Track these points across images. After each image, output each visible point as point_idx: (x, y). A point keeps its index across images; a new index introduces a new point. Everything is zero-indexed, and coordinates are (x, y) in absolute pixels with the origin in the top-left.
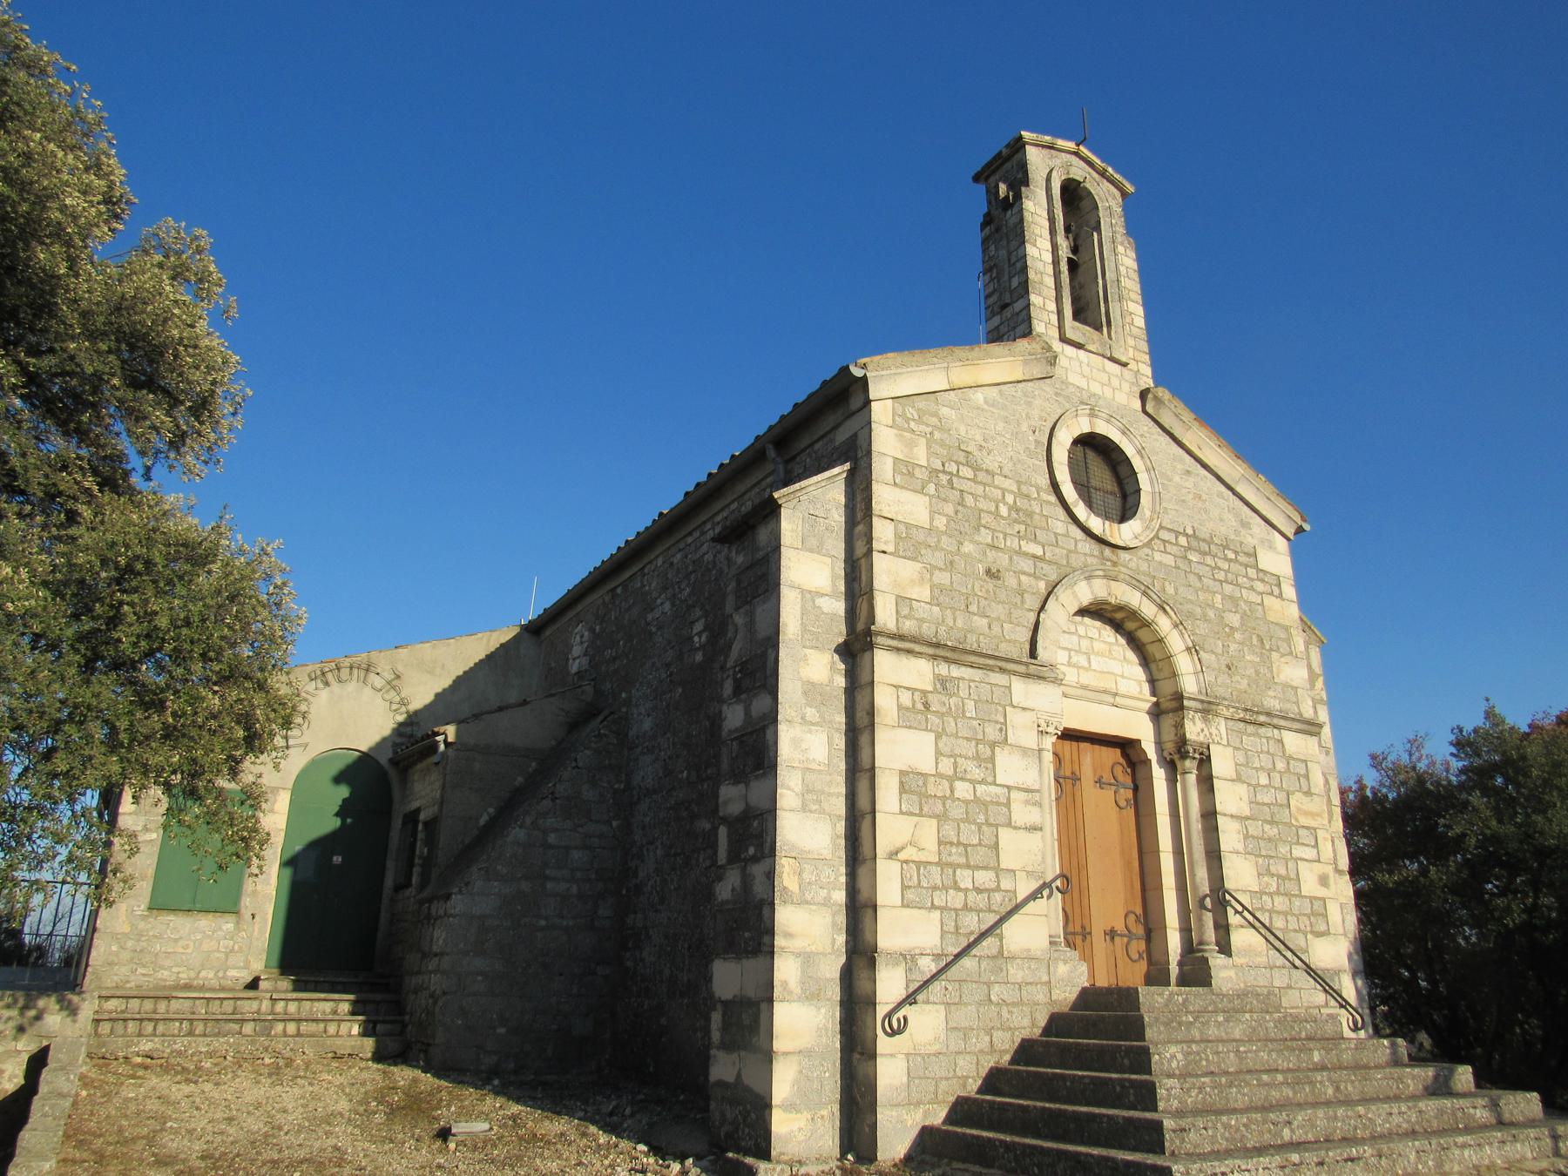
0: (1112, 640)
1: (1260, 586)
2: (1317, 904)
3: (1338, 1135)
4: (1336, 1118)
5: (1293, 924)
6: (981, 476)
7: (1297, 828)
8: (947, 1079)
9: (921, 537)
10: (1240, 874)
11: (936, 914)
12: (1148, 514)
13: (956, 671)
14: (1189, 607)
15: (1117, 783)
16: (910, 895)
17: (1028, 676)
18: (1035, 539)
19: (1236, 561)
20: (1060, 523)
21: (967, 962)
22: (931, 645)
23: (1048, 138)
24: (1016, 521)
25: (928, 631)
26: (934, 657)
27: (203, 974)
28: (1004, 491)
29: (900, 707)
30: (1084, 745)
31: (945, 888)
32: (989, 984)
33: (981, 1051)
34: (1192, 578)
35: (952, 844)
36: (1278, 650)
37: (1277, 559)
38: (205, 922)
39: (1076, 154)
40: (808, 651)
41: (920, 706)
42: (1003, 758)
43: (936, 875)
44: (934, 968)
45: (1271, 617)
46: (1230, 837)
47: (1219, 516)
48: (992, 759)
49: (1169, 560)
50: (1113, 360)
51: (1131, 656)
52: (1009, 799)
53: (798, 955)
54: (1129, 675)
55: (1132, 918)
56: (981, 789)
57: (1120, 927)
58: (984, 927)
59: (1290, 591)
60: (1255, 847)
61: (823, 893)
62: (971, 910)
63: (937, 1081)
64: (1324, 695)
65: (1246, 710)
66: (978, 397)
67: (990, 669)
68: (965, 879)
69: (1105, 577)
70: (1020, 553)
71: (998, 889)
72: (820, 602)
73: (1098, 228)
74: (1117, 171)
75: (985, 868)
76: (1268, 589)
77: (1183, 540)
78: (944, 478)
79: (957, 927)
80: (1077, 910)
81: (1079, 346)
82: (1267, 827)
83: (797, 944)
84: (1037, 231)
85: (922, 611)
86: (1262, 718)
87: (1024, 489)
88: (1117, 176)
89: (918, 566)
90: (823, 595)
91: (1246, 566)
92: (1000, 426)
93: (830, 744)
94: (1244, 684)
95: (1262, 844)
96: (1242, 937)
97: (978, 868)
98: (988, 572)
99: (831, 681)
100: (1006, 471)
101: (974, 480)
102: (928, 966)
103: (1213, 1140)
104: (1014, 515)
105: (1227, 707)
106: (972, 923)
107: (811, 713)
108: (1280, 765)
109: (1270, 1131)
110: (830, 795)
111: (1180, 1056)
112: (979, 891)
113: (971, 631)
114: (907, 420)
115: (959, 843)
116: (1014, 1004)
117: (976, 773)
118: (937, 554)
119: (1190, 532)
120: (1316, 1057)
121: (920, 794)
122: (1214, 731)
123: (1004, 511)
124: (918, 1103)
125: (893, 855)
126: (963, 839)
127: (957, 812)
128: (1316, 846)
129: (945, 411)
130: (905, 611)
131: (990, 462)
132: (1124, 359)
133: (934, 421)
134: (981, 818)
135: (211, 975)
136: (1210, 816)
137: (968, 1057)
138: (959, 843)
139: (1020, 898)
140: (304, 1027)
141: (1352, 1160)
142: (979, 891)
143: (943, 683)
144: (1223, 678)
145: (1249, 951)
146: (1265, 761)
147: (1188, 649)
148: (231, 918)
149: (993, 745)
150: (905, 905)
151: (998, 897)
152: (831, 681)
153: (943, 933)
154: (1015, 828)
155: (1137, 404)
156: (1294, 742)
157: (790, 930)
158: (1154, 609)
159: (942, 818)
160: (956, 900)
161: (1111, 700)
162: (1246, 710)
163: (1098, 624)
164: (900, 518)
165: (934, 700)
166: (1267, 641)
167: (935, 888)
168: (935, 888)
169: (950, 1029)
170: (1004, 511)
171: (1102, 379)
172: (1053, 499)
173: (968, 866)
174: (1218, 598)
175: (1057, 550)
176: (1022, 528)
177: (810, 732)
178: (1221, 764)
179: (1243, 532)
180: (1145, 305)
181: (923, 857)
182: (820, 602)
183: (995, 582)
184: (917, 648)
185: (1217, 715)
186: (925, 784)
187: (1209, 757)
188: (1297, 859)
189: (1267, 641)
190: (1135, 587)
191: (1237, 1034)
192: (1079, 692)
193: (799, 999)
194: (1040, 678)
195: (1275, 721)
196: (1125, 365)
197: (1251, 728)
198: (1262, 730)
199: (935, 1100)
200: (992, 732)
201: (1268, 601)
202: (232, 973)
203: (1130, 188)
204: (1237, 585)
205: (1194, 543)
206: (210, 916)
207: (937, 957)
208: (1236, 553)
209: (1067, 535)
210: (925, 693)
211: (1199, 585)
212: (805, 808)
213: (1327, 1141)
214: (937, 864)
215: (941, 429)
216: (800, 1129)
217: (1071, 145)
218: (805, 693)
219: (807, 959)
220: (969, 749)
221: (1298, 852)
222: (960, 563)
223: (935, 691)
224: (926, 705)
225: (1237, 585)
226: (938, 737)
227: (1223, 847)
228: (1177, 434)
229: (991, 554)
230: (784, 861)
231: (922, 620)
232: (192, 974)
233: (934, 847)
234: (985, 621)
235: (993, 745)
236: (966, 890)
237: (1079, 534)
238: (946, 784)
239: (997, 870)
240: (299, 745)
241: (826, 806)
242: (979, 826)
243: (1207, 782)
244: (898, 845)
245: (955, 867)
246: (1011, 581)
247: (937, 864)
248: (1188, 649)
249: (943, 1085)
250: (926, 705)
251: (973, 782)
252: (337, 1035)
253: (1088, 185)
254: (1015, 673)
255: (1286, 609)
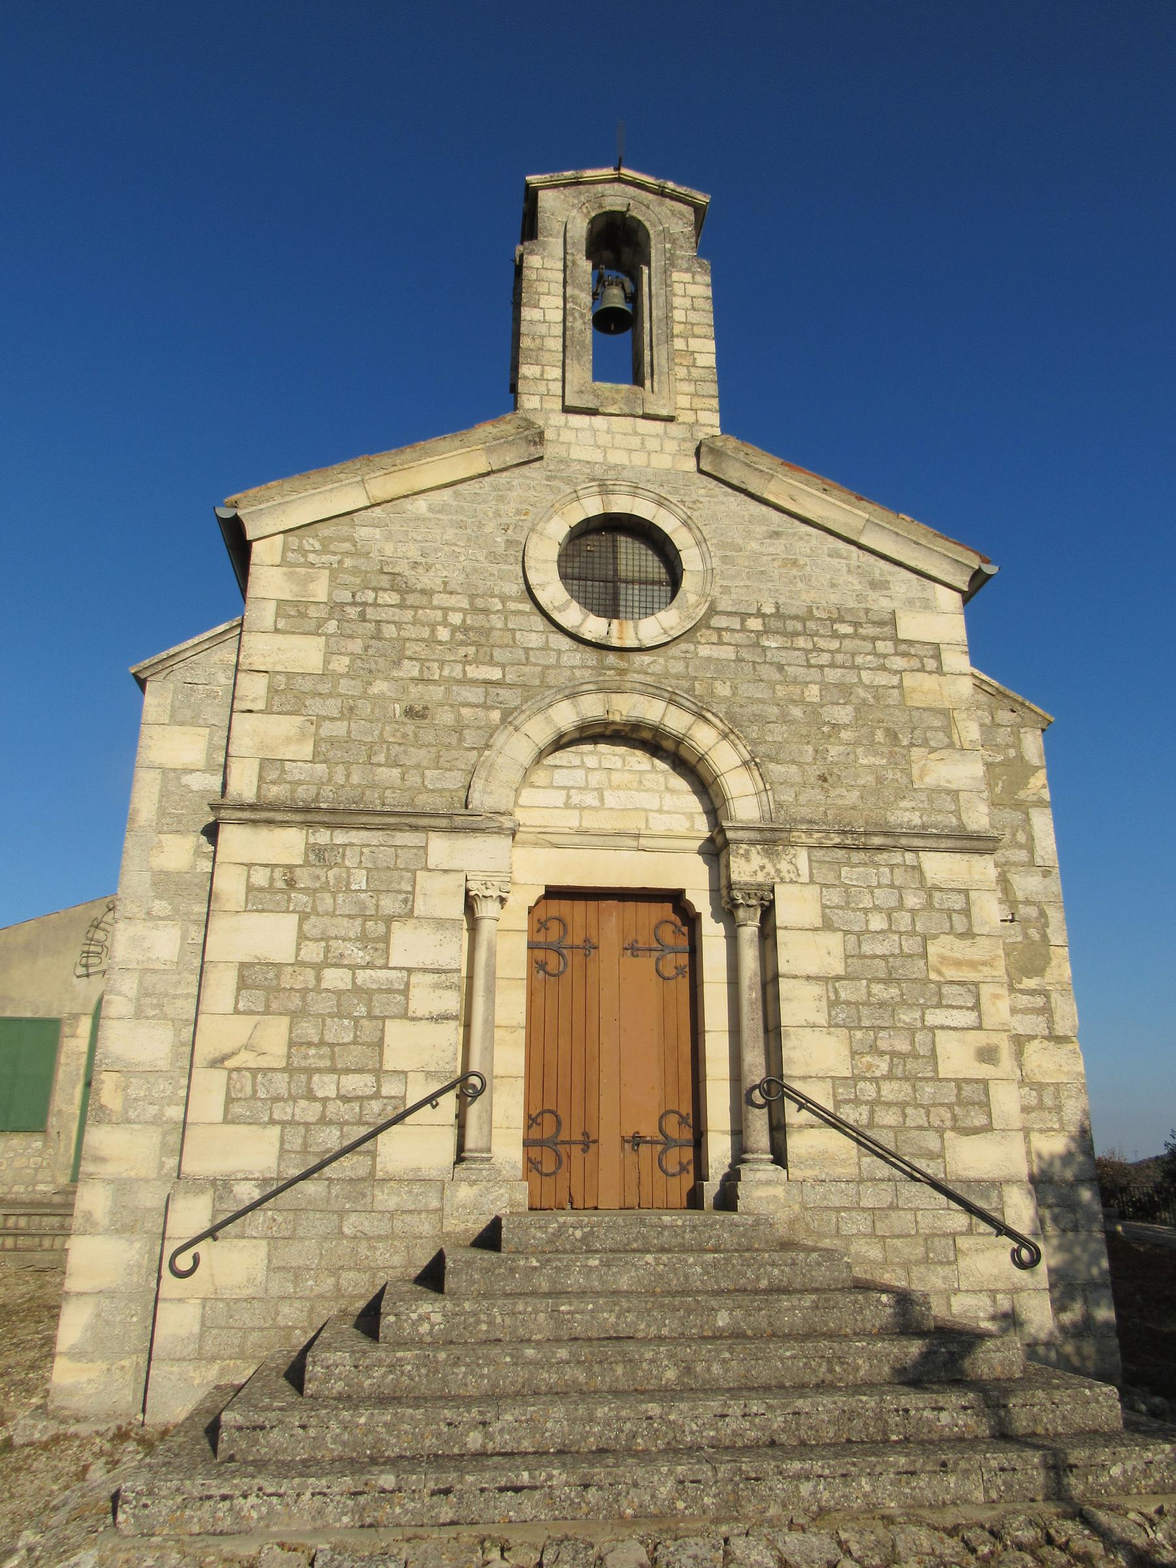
0: (647, 767)
1: (898, 663)
2: (967, 1091)
3: (592, 1443)
4: (591, 1419)
5: (916, 1117)
6: (411, 599)
7: (939, 984)
8: (261, 1329)
9: (307, 685)
10: (815, 1055)
11: (276, 1131)
12: (692, 598)
13: (340, 837)
14: (756, 708)
15: (663, 947)
16: (238, 1109)
17: (454, 830)
18: (492, 662)
19: (855, 635)
20: (534, 634)
21: (309, 1187)
22: (297, 810)
23: (568, 174)
24: (462, 643)
25: (304, 793)
26: (308, 824)
27: (15, 1188)
28: (446, 610)
29: (250, 888)
30: (605, 904)
31: (294, 1099)
32: (342, 1214)
33: (321, 1296)
34: (767, 672)
35: (310, 1044)
36: (925, 743)
37: (942, 621)
38: (17, 1141)
39: (619, 180)
40: (163, 837)
41: (280, 884)
42: (401, 935)
43: (281, 1083)
44: (257, 1195)
45: (916, 700)
46: (799, 1005)
47: (827, 576)
48: (386, 939)
49: (727, 653)
50: (646, 417)
51: (680, 783)
52: (407, 984)
53: (110, 1182)
54: (682, 810)
55: (673, 1119)
56: (363, 976)
57: (649, 1129)
58: (346, 1143)
59: (958, 660)
60: (842, 1015)
61: (153, 1110)
62: (331, 1123)
63: (246, 1331)
64: (1046, 795)
65: (844, 832)
66: (420, 505)
67: (396, 828)
68: (326, 1086)
69: (599, 690)
70: (465, 681)
71: (377, 1095)
72: (187, 779)
73: (649, 264)
74: (679, 182)
75: (360, 1071)
76: (915, 663)
77: (755, 624)
78: (352, 612)
79: (305, 1145)
80: (577, 1111)
81: (592, 412)
82: (876, 988)
83: (108, 1170)
84: (543, 287)
85: (296, 772)
86: (877, 841)
87: (480, 603)
88: (682, 190)
89: (298, 720)
90: (192, 771)
91: (874, 639)
92: (450, 534)
93: (184, 938)
94: (853, 797)
95: (865, 1011)
96: (808, 1141)
97: (348, 1071)
98: (410, 712)
99: (194, 866)
100: (452, 586)
101: (401, 606)
102: (248, 1192)
103: (318, 1443)
104: (460, 636)
105: (809, 832)
106: (331, 1139)
107: (160, 907)
108: (913, 900)
109: (439, 1435)
110: (175, 997)
111: (437, 1318)
112: (345, 1099)
113: (373, 786)
114: (305, 553)
115: (322, 1043)
116: (380, 1238)
117: (359, 956)
118: (331, 702)
119: (768, 609)
120: (722, 1320)
121: (268, 989)
122: (784, 866)
123: (443, 634)
124: (213, 1359)
125: (217, 1062)
126: (329, 1038)
127: (322, 1005)
128: (977, 1007)
129: (363, 532)
130: (273, 775)
131: (427, 581)
132: (664, 412)
133: (347, 546)
134: (362, 1010)
135: (22, 1189)
136: (770, 981)
137: (298, 1304)
138: (322, 1043)
139: (410, 1104)
140: (22, 1242)
141: (517, 1490)
142: (345, 1099)
143: (319, 855)
144: (816, 795)
145: (822, 1158)
146: (885, 898)
147: (745, 763)
148: (38, 1136)
149: (389, 920)
150: (228, 1119)
151: (375, 1106)
152: (194, 866)
153: (283, 1152)
154: (413, 1019)
155: (690, 464)
156: (940, 867)
157: (104, 1153)
158: (688, 719)
159: (295, 1015)
160: (308, 1111)
161: (634, 843)
162: (844, 832)
163: (622, 750)
164: (279, 668)
165: (304, 879)
166: (909, 731)
167: (277, 1099)
168: (277, 1099)
169: (271, 1269)
170: (443, 634)
171: (639, 448)
172: (528, 607)
173: (333, 1070)
174: (814, 689)
175: (526, 669)
176: (471, 650)
177: (157, 927)
178: (792, 908)
179: (872, 595)
180: (719, 338)
181: (263, 1062)
182: (187, 779)
183: (418, 722)
184: (279, 817)
185: (794, 845)
186: (278, 976)
187: (772, 902)
188: (933, 1029)
189: (909, 731)
190: (654, 696)
191: (624, 1283)
192: (577, 839)
193: (106, 1232)
194: (475, 830)
195: (904, 841)
196: (670, 419)
197: (857, 857)
198: (882, 857)
199: (241, 1355)
200: (389, 904)
201: (909, 680)
202: (41, 1187)
203: (702, 198)
204: (854, 667)
205: (774, 624)
206: (21, 1135)
207: (266, 1181)
208: (856, 625)
209: (546, 648)
210: (290, 868)
211: (778, 677)
212: (139, 1014)
213: (560, 1452)
214: (283, 1070)
215: (355, 554)
216: (89, 1381)
217: (608, 172)
218: (154, 884)
219: (122, 1186)
220: (354, 928)
221: (934, 1017)
222: (365, 708)
223: (307, 863)
224: (291, 883)
225: (854, 667)
226: (304, 917)
227: (784, 1021)
228: (752, 489)
229: (415, 691)
230: (105, 1076)
231: (299, 783)
232: (6, 1189)
233: (282, 1050)
234: (396, 772)
235: (389, 920)
236: (325, 1100)
237: (565, 643)
238: (310, 974)
239: (379, 1073)
240: (97, 973)
241: (168, 1010)
242: (356, 1020)
243: (767, 933)
244: (227, 1050)
245: (310, 1072)
246: (446, 717)
247: (283, 1070)
248: (745, 763)
249: (254, 1337)
250: (291, 883)
251: (353, 968)
252: (51, 1250)
253: (634, 213)
254: (435, 829)
255: (958, 680)
